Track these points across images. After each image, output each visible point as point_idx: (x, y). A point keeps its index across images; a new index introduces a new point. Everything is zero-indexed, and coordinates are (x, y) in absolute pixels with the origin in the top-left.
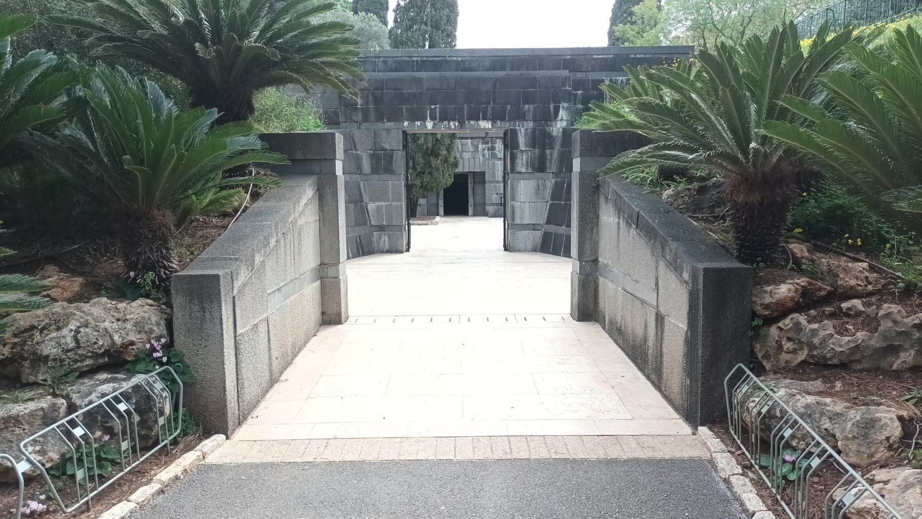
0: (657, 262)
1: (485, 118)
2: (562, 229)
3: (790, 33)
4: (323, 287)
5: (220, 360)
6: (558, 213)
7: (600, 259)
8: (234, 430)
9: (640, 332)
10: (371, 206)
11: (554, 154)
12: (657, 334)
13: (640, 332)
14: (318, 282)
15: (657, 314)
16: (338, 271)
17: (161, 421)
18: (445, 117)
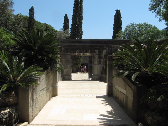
0: (126, 85)
1: (88, 53)
2: (104, 75)
3: (146, 23)
4: (53, 88)
5: (81, 36)
6: (104, 72)
7: (113, 83)
8: (31, 122)
9: (122, 100)
10: (65, 70)
11: (102, 60)
12: (126, 99)
13: (122, 100)
14: (52, 87)
15: (126, 96)
16: (56, 85)
17: (14, 120)
18: (80, 52)
